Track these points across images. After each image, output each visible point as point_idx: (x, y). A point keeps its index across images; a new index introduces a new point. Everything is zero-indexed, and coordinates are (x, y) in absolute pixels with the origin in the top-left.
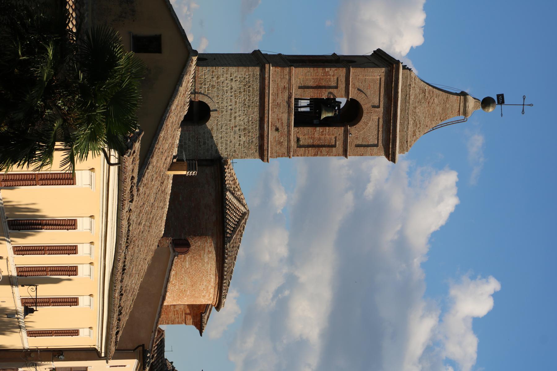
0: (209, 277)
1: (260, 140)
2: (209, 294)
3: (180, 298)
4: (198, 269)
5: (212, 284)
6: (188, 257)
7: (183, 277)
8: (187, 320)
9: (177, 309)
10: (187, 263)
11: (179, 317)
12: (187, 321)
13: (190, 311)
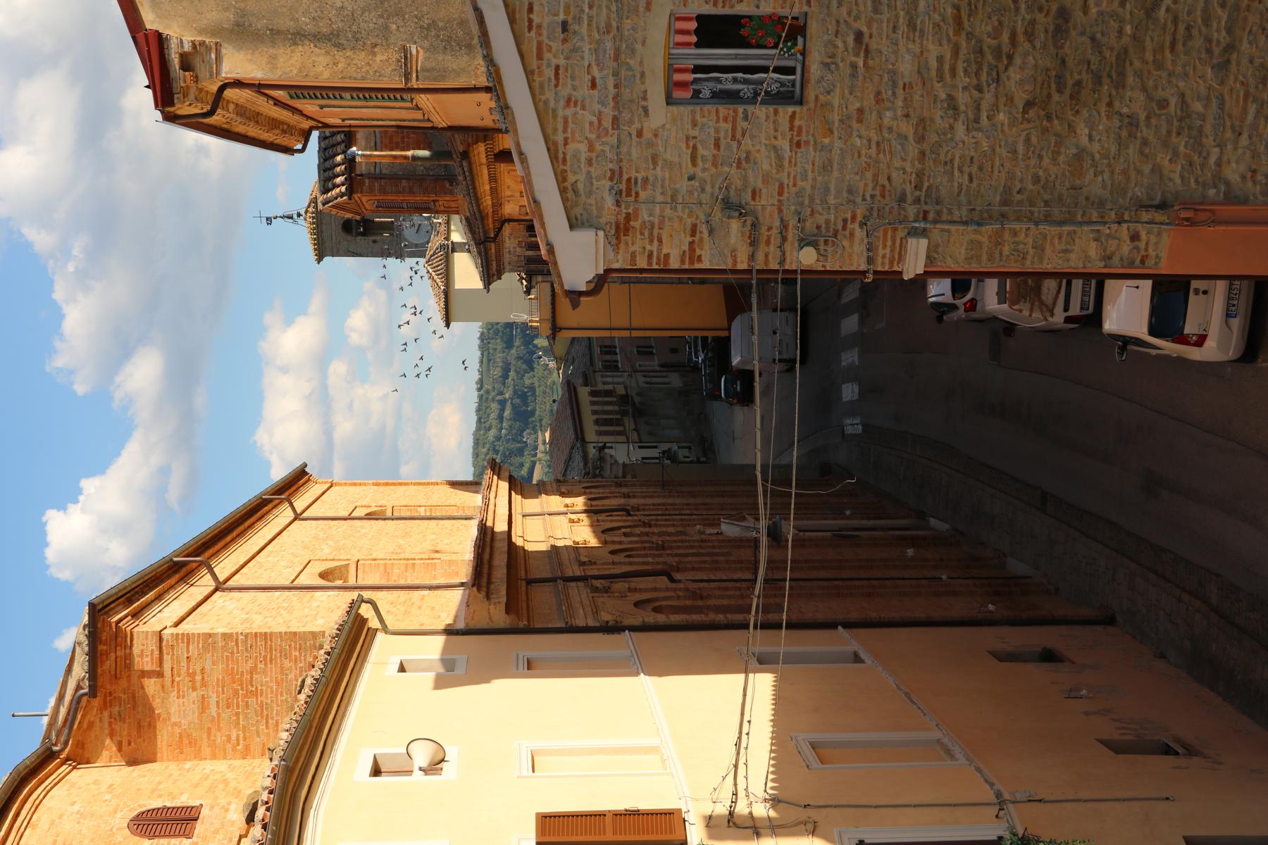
8: (152, 651)
9: (194, 694)
11: (184, 663)
12: (152, 645)
13: (143, 688)
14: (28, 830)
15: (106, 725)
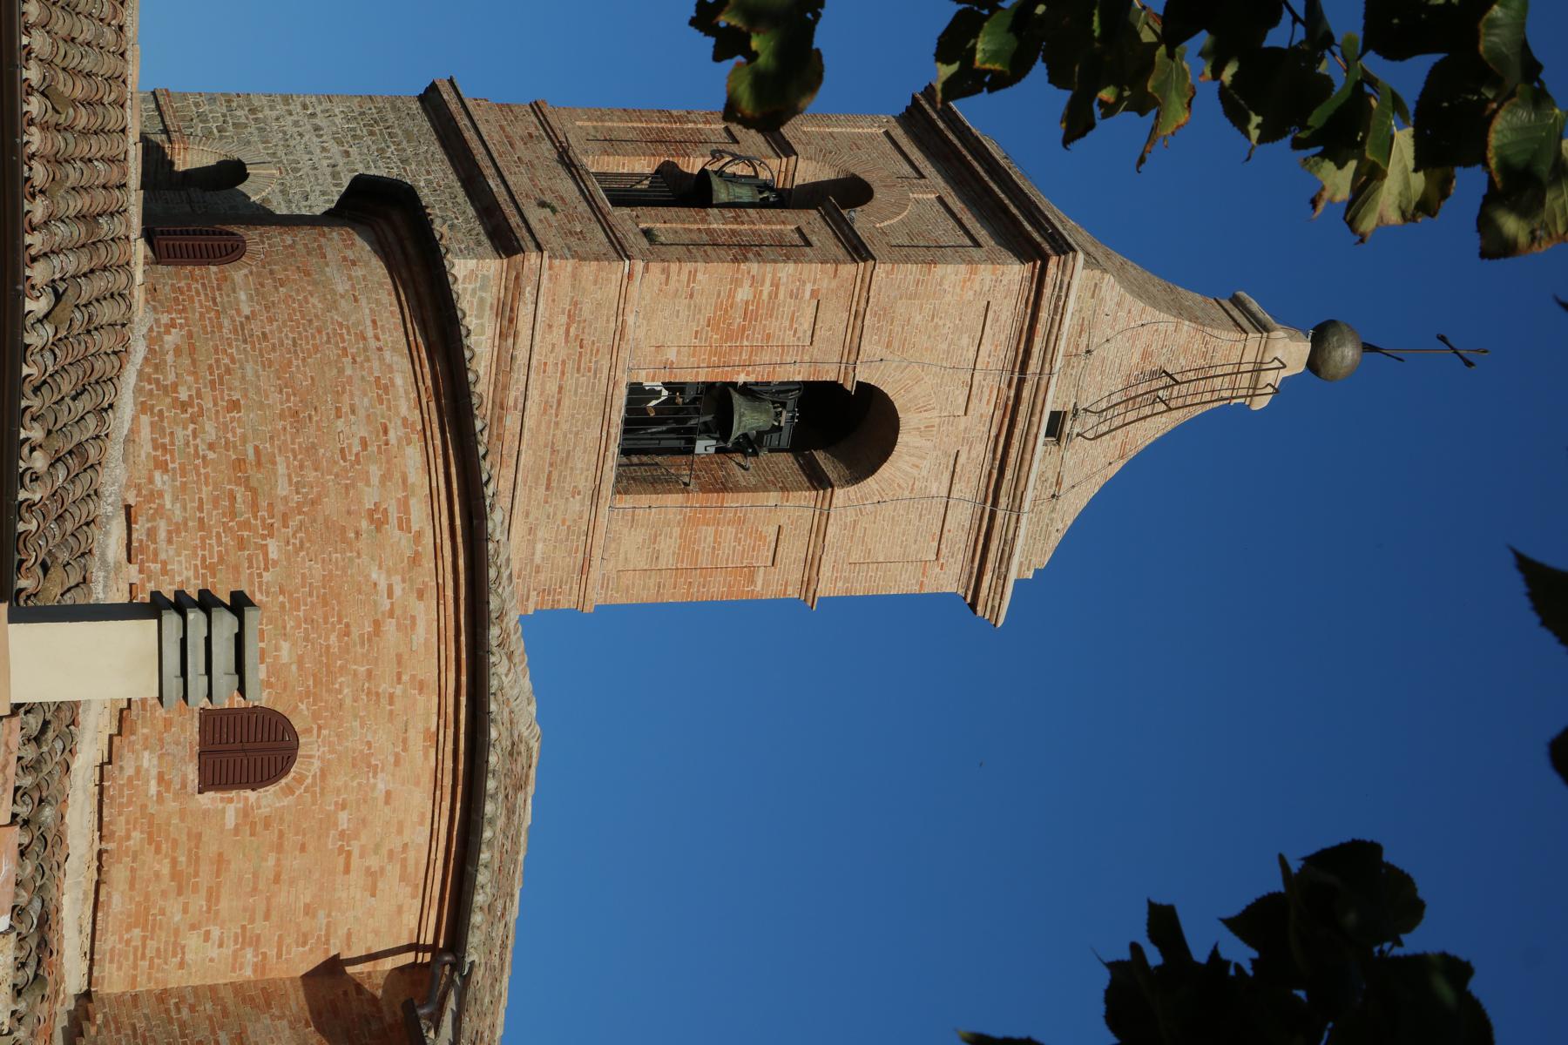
0: (376, 364)
1: (485, 220)
2: (401, 495)
3: (242, 544)
4: (310, 321)
5: (404, 411)
6: (239, 273)
7: (233, 361)
10: (243, 296)
14: (434, 728)
15: (385, 1008)
